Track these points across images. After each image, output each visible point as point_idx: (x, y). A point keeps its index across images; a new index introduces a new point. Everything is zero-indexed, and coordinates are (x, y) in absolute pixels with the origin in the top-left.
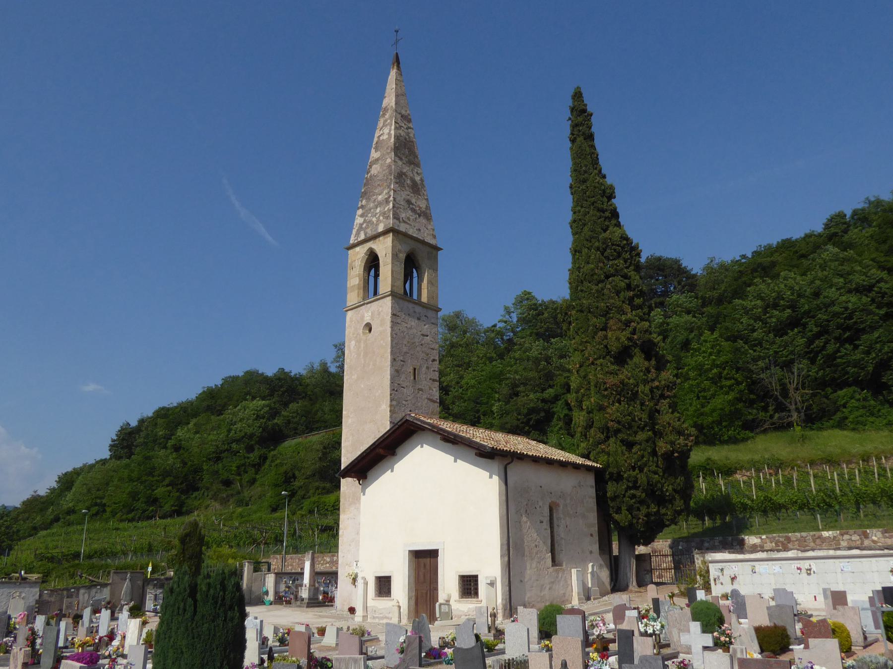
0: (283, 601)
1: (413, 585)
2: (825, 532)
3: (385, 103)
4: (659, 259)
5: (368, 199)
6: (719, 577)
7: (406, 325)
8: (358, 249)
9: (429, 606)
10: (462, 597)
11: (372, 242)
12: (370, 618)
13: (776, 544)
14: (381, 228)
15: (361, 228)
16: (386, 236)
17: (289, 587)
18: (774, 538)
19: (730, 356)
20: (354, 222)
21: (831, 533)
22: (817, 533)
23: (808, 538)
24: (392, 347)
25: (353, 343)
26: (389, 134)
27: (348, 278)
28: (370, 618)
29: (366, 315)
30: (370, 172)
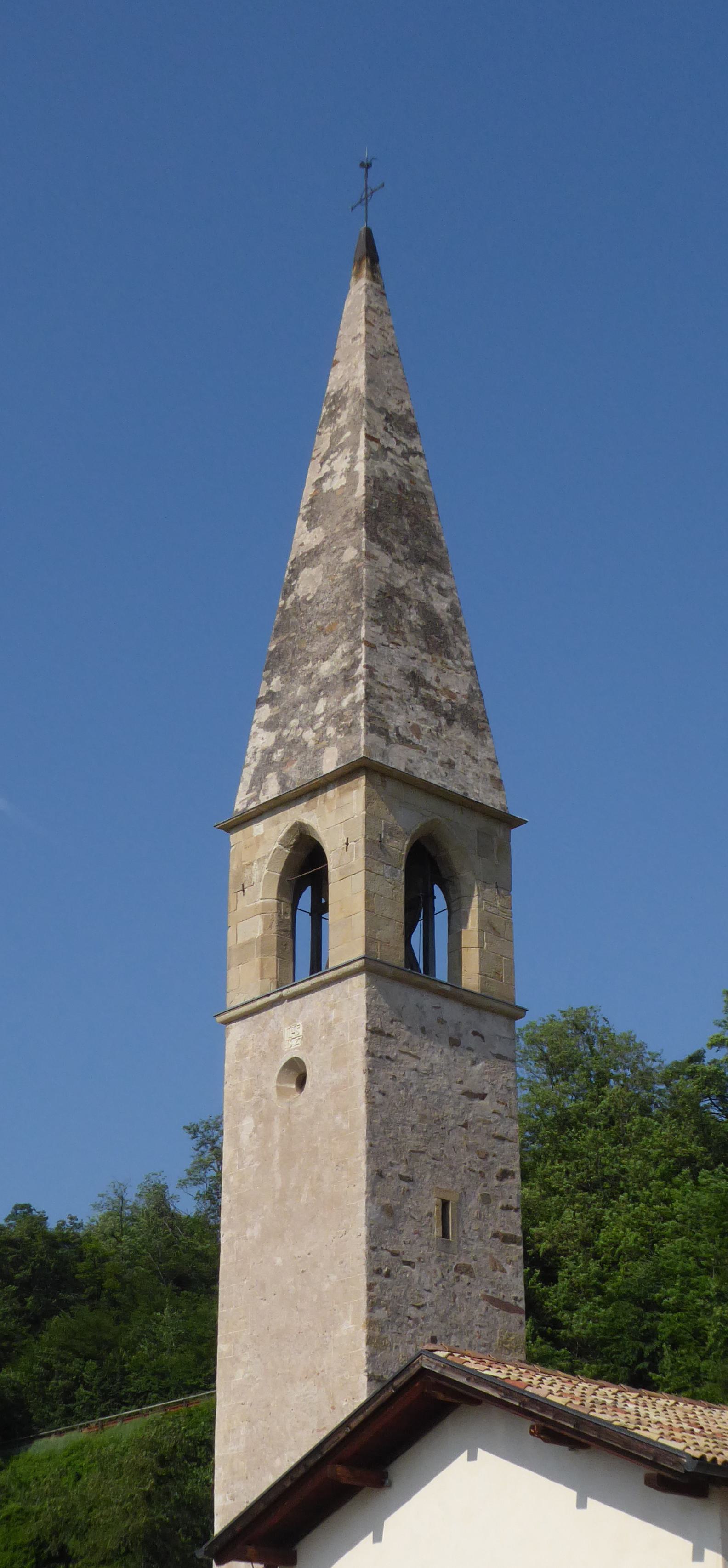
3: (336, 379)
5: (290, 674)
8: (258, 828)
11: (302, 806)
14: (330, 763)
15: (267, 763)
20: (246, 746)
24: (372, 1132)
25: (248, 1123)
26: (350, 473)
29: (287, 1033)
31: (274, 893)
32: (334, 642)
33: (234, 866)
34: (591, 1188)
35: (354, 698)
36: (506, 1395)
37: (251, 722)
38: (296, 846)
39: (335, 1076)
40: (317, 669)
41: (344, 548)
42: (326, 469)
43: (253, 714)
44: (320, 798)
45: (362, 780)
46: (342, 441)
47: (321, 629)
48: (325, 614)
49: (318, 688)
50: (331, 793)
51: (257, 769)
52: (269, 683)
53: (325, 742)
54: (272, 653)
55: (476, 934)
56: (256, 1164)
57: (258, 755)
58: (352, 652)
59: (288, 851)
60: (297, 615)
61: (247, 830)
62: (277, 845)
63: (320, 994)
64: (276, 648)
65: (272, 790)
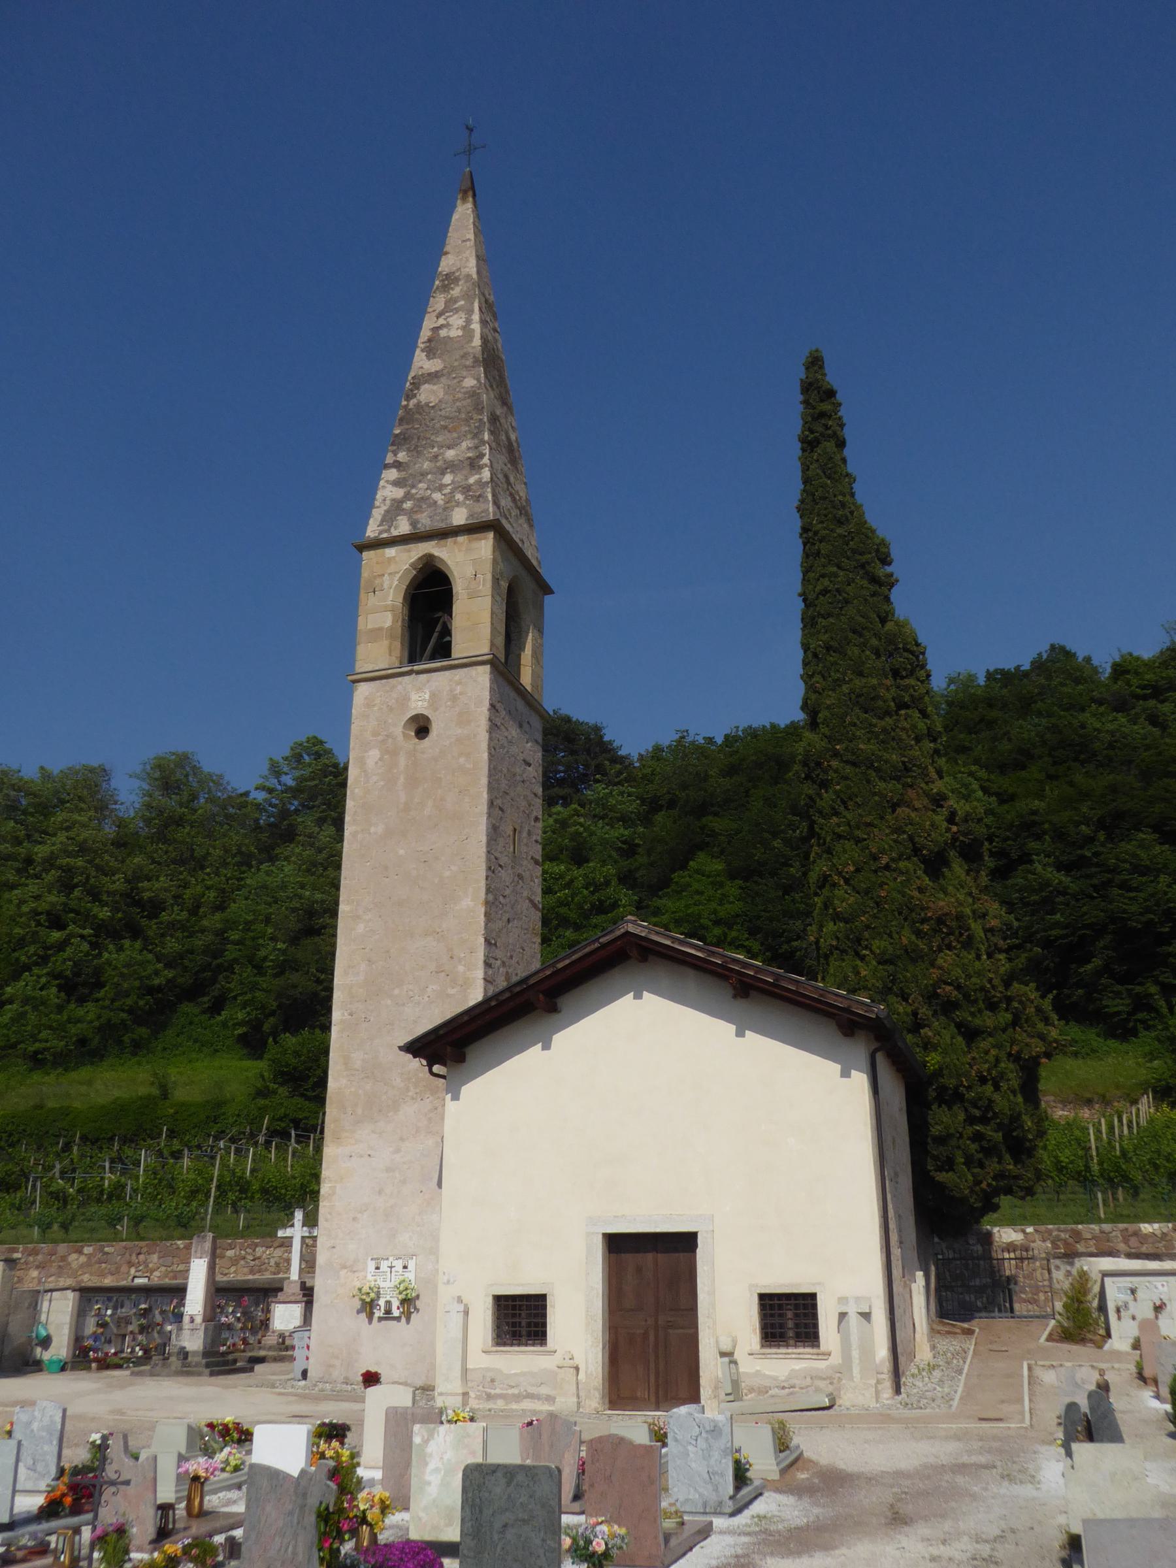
0: (91, 1361)
1: (607, 1315)
2: (1146, 1225)
3: (446, 264)
4: (567, 720)
5: (416, 452)
6: (1126, 1306)
7: (506, 734)
8: (391, 552)
9: (652, 1365)
10: (498, 1344)
11: (433, 543)
12: (478, 1398)
13: (1053, 1243)
14: (459, 517)
15: (396, 508)
16: (475, 536)
17: (104, 1325)
18: (1050, 1232)
19: (740, 904)
20: (376, 494)
21: (1156, 1226)
22: (1131, 1227)
23: (1114, 1233)
24: (493, 773)
25: (374, 754)
26: (466, 328)
27: (361, 610)
28: (478, 1398)
29: (414, 696)
30: (415, 396)
31: (401, 600)
32: (459, 438)
33: (365, 574)
34: (182, 862)
35: (481, 479)
36: (709, 956)
37: (379, 480)
38: (420, 571)
39: (459, 731)
40: (443, 454)
41: (464, 378)
42: (441, 321)
43: (381, 473)
44: (450, 540)
45: (491, 535)
46: (456, 306)
47: (445, 427)
48: (447, 418)
49: (444, 466)
50: (460, 539)
51: (387, 512)
52: (395, 455)
53: (454, 503)
54: (397, 435)
55: (530, 657)
56: (382, 783)
57: (388, 502)
58: (476, 447)
59: (415, 572)
60: (420, 414)
61: (379, 551)
62: (407, 566)
63: (447, 673)
64: (400, 433)
65: (403, 527)
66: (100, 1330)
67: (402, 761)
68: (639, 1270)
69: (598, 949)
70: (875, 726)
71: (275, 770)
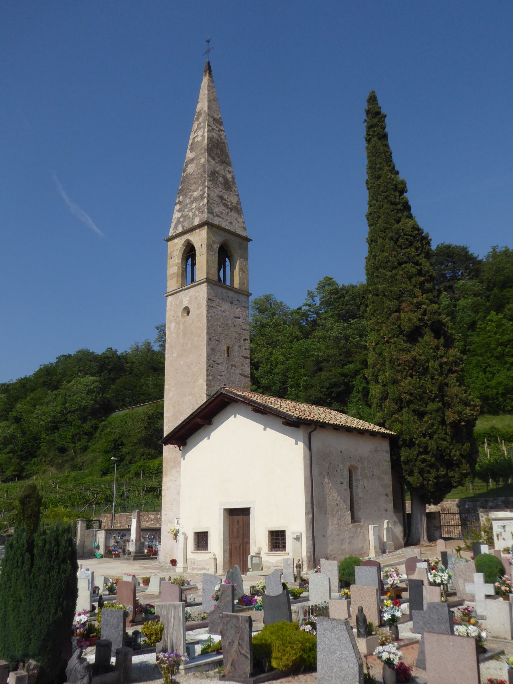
4: (449, 247)
5: (185, 196)
6: (501, 534)
8: (176, 241)
9: (242, 558)
11: (188, 234)
12: (190, 569)
14: (197, 222)
15: (178, 222)
17: (118, 542)
25: (173, 325)
26: (203, 136)
27: (168, 266)
28: (190, 569)
29: (184, 300)
31: (181, 260)
33: (169, 252)
44: (194, 232)
45: (206, 227)
47: (194, 183)
48: (195, 178)
50: (197, 231)
51: (176, 224)
54: (180, 190)
55: (238, 272)
58: (203, 189)
65: (180, 230)
66: (116, 544)
67: (181, 326)
68: (238, 522)
69: (213, 400)
70: (386, 275)
71: (311, 296)
